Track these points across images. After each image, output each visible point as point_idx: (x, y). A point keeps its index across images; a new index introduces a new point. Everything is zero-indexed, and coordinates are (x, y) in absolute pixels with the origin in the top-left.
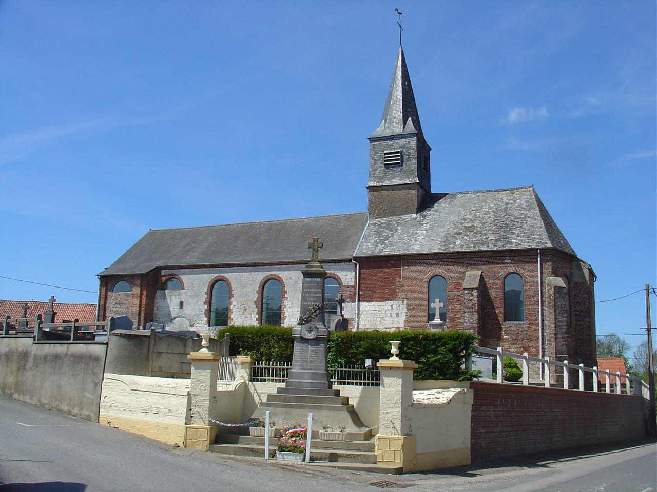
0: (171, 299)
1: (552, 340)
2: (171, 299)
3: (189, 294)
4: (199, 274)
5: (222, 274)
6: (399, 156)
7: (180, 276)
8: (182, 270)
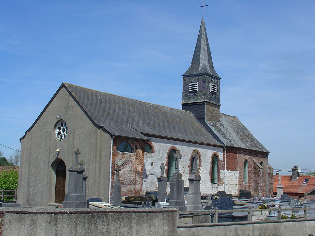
0: (146, 160)
1: (112, 210)
2: (146, 160)
3: (157, 158)
4: (164, 143)
5: (175, 145)
6: (190, 87)
7: (152, 143)
8: (153, 138)
